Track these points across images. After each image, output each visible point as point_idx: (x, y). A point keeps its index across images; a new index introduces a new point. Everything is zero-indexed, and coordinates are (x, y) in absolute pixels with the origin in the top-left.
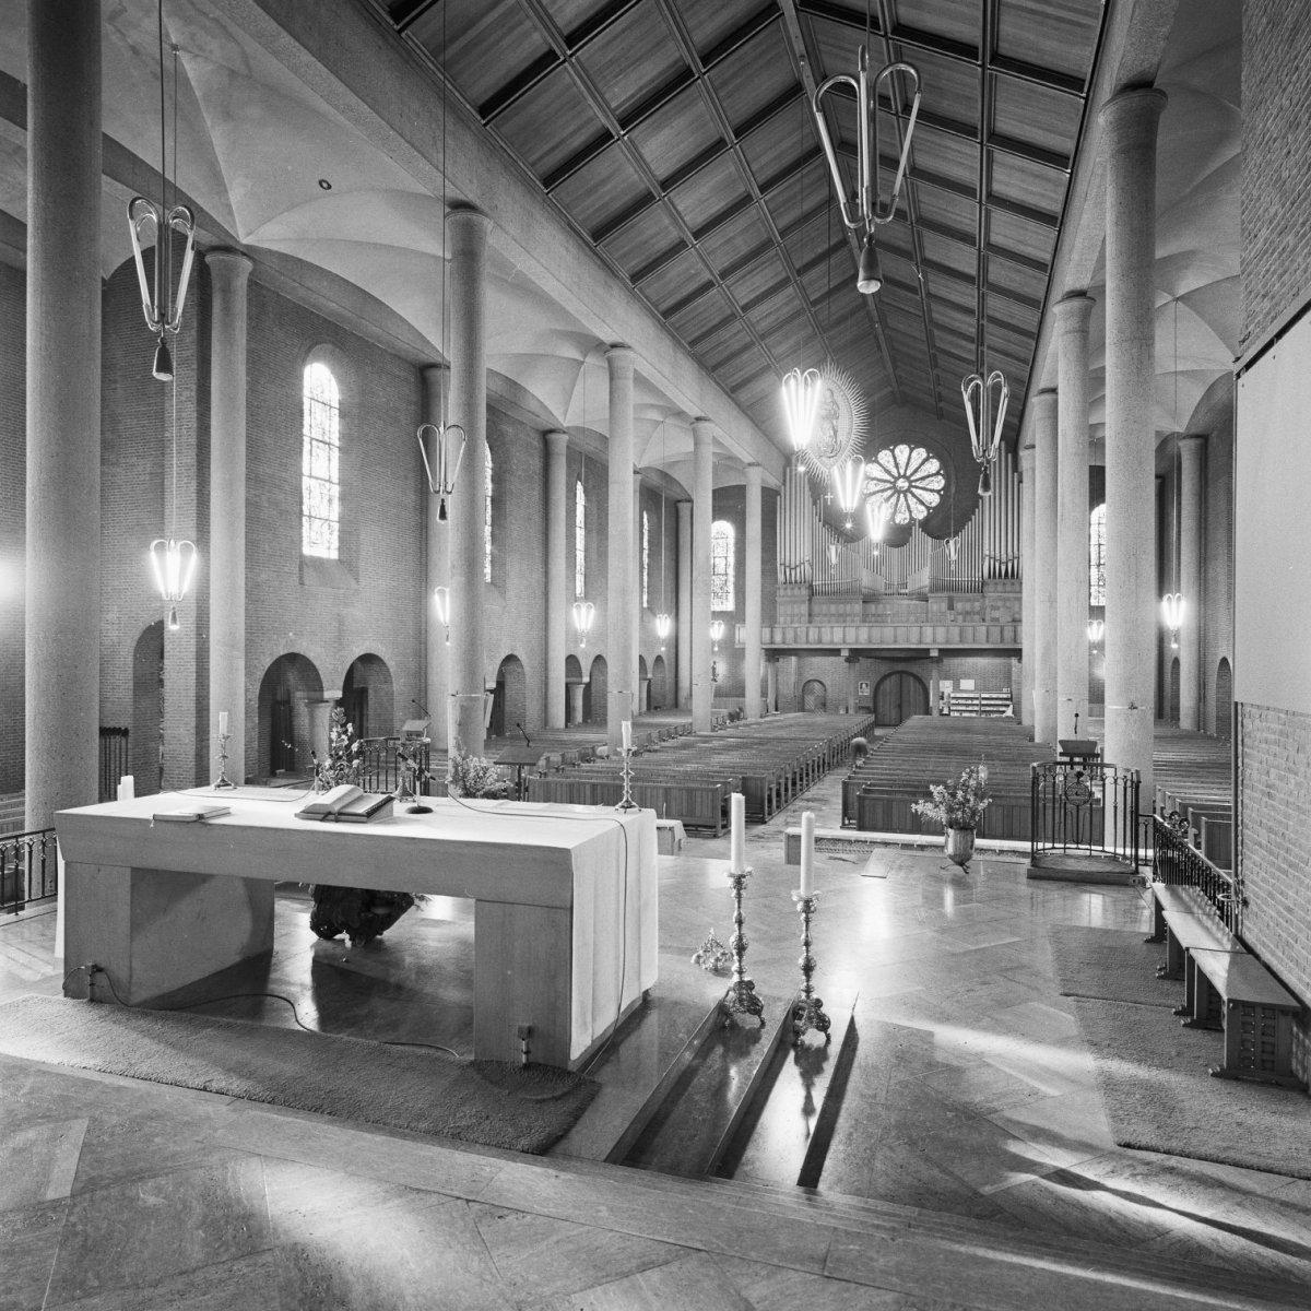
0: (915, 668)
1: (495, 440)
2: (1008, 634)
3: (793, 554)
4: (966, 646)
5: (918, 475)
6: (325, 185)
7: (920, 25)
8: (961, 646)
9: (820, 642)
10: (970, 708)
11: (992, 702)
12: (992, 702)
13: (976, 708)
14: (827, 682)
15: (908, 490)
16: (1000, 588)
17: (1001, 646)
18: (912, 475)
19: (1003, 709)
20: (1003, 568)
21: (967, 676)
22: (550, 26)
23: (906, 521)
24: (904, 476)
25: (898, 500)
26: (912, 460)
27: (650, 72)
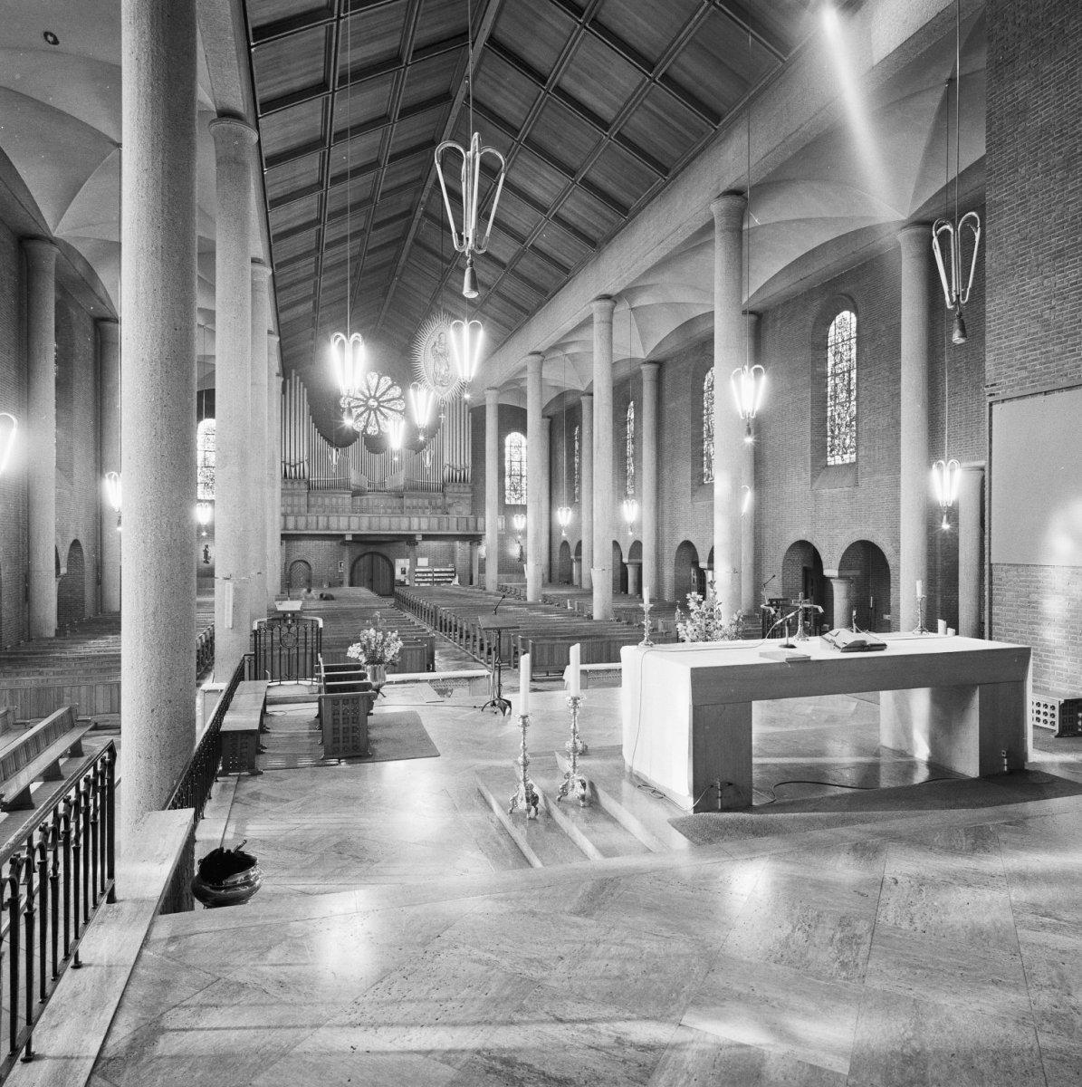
0: (384, 550)
1: (62, 321)
2: (471, 524)
3: (293, 452)
4: (443, 533)
5: (385, 398)
6: (50, 38)
7: (574, 94)
8: (439, 533)
9: (328, 528)
10: (426, 580)
11: (442, 575)
12: (442, 575)
13: (430, 580)
14: (312, 561)
15: (377, 408)
16: (456, 489)
17: (467, 533)
18: (380, 396)
19: (450, 579)
20: (458, 474)
21: (423, 555)
22: (629, 105)
23: (376, 433)
24: (374, 397)
25: (369, 416)
26: (381, 385)
27: (375, 50)
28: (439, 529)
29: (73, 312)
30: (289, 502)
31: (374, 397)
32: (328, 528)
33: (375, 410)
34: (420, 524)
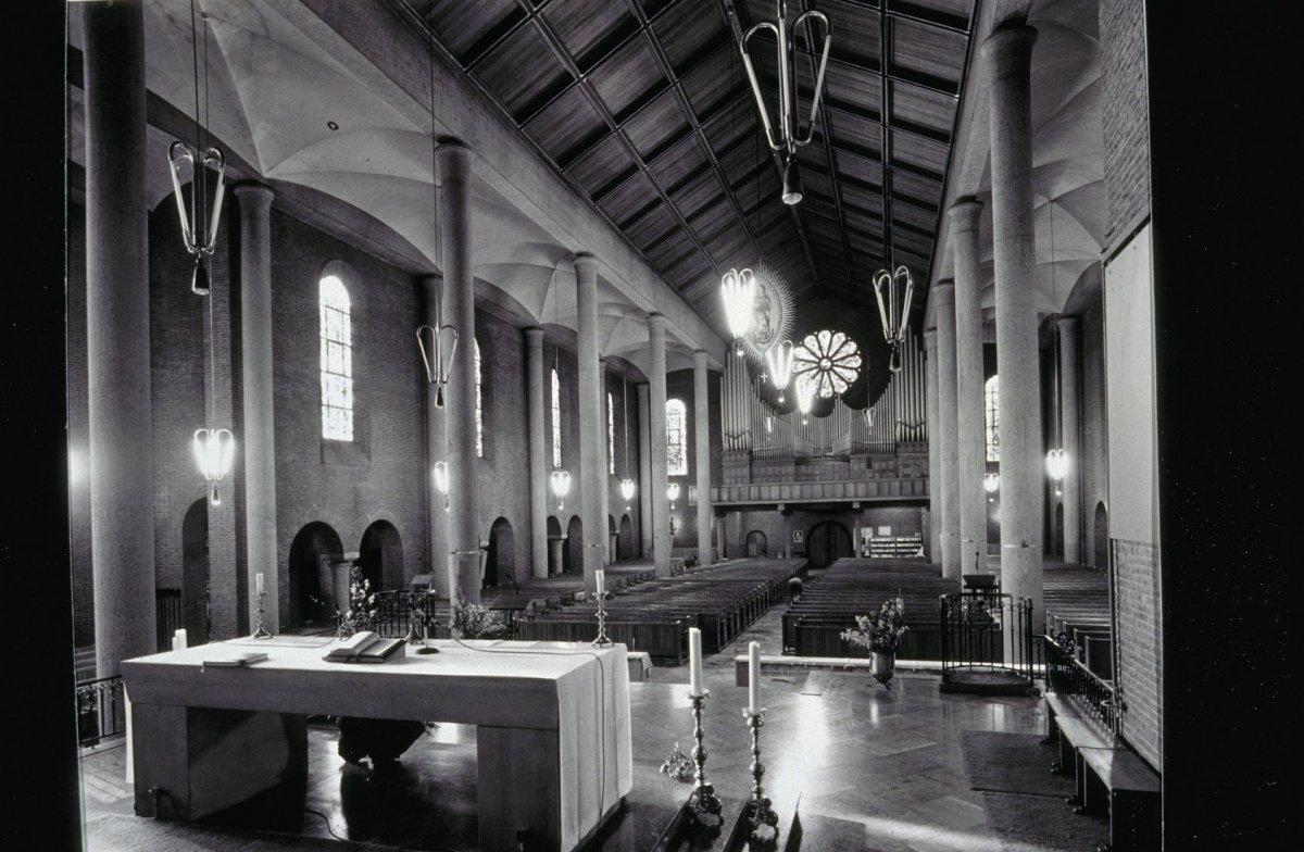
0: (841, 519)
4: (883, 499)
5: (839, 356)
6: (333, 126)
8: (878, 499)
9: (760, 499)
11: (906, 545)
12: (906, 545)
13: (892, 551)
14: (767, 533)
15: (831, 369)
16: (910, 449)
21: (885, 524)
23: (830, 395)
24: (827, 357)
26: (833, 343)
28: (739, 499)
29: (494, 328)
30: (734, 474)
31: (827, 357)
32: (760, 499)
33: (828, 371)
34: (856, 490)
